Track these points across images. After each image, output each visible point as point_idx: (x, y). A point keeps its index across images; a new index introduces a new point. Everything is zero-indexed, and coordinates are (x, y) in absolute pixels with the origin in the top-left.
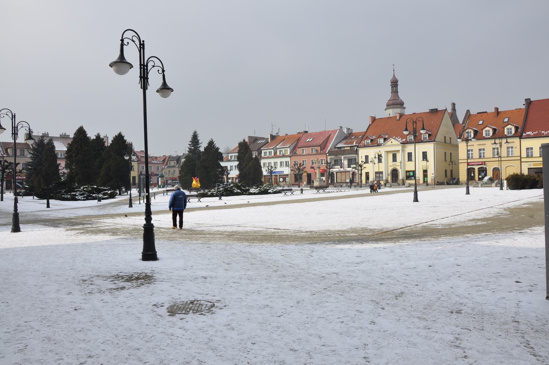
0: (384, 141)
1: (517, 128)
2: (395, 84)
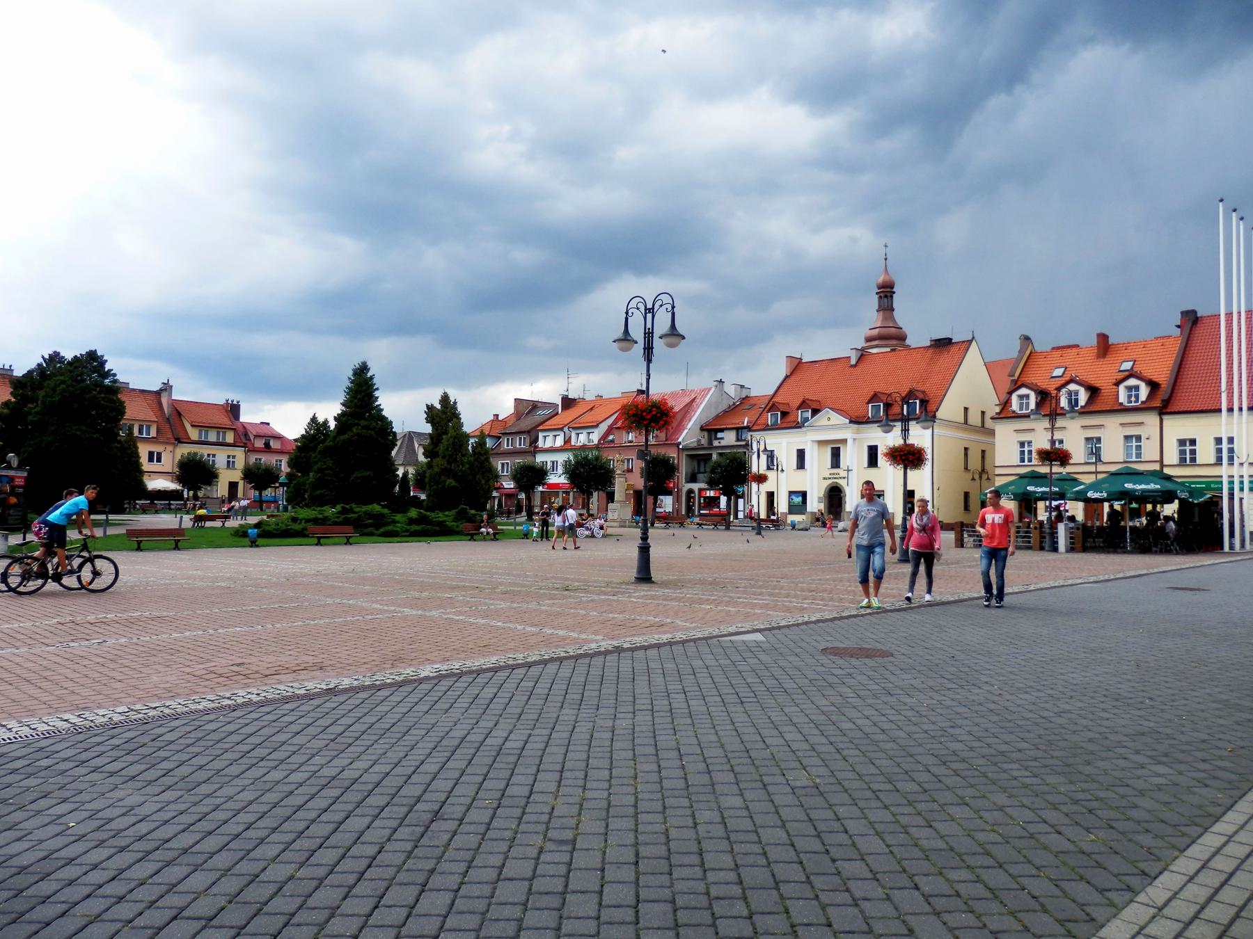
0: (813, 415)
1: (1154, 386)
2: (886, 292)
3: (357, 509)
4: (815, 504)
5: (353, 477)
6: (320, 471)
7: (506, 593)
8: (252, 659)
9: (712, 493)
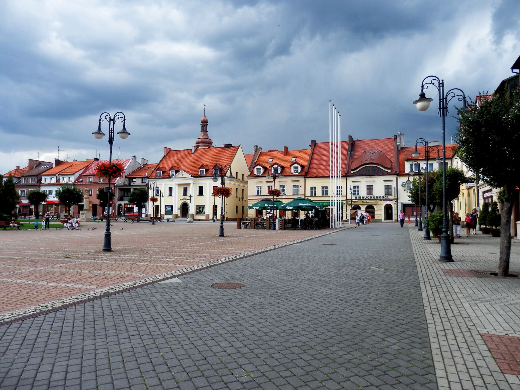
1: (303, 167)
2: (205, 124)
4: (176, 211)
7: (31, 261)
9: (130, 206)
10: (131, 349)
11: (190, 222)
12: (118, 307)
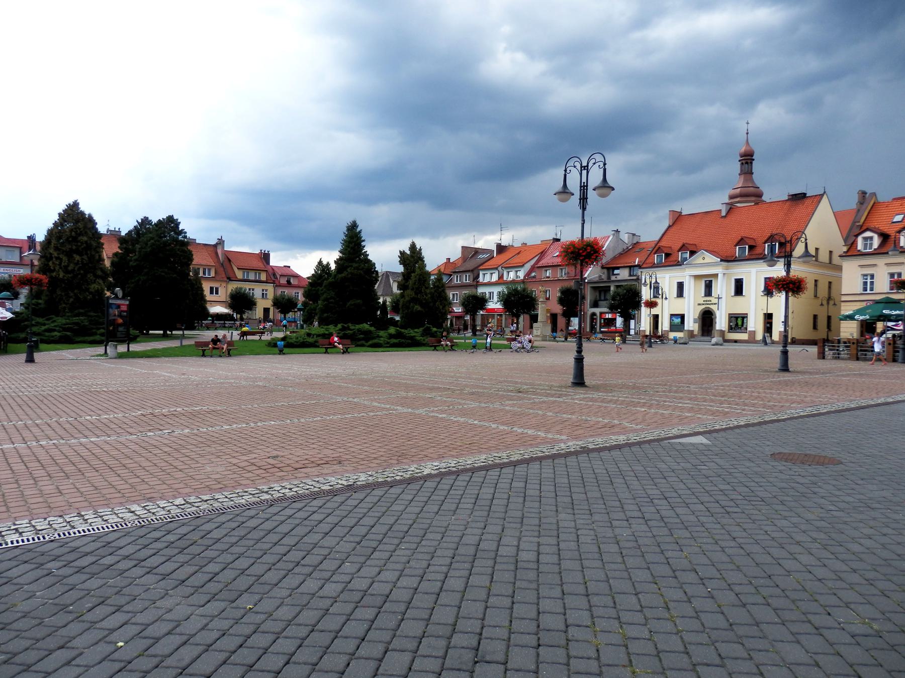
0: (691, 255)
2: (747, 159)
3: (352, 327)
4: (691, 324)
5: (349, 304)
6: (326, 300)
7: (473, 394)
8: (286, 453)
9: (610, 316)
10: (632, 538)
11: (717, 344)
12: (605, 471)
